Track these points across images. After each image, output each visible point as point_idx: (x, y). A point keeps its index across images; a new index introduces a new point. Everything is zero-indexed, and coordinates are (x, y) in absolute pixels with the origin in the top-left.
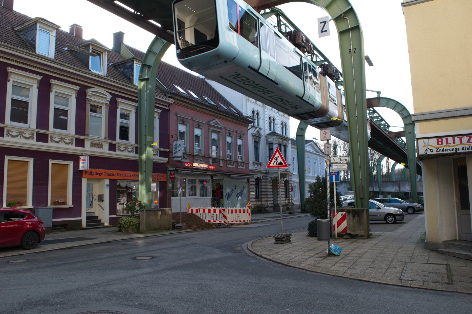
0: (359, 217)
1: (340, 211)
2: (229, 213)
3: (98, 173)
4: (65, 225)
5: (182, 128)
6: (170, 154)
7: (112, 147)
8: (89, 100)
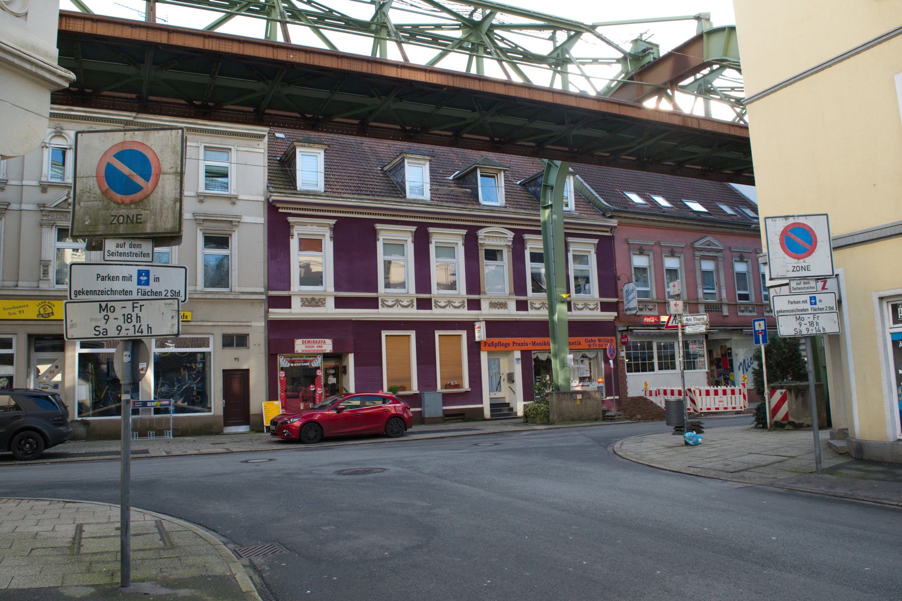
0: (803, 396)
1: (778, 389)
2: (700, 395)
3: (503, 344)
4: (463, 415)
5: (639, 261)
6: (620, 305)
7: (522, 306)
8: (482, 245)
